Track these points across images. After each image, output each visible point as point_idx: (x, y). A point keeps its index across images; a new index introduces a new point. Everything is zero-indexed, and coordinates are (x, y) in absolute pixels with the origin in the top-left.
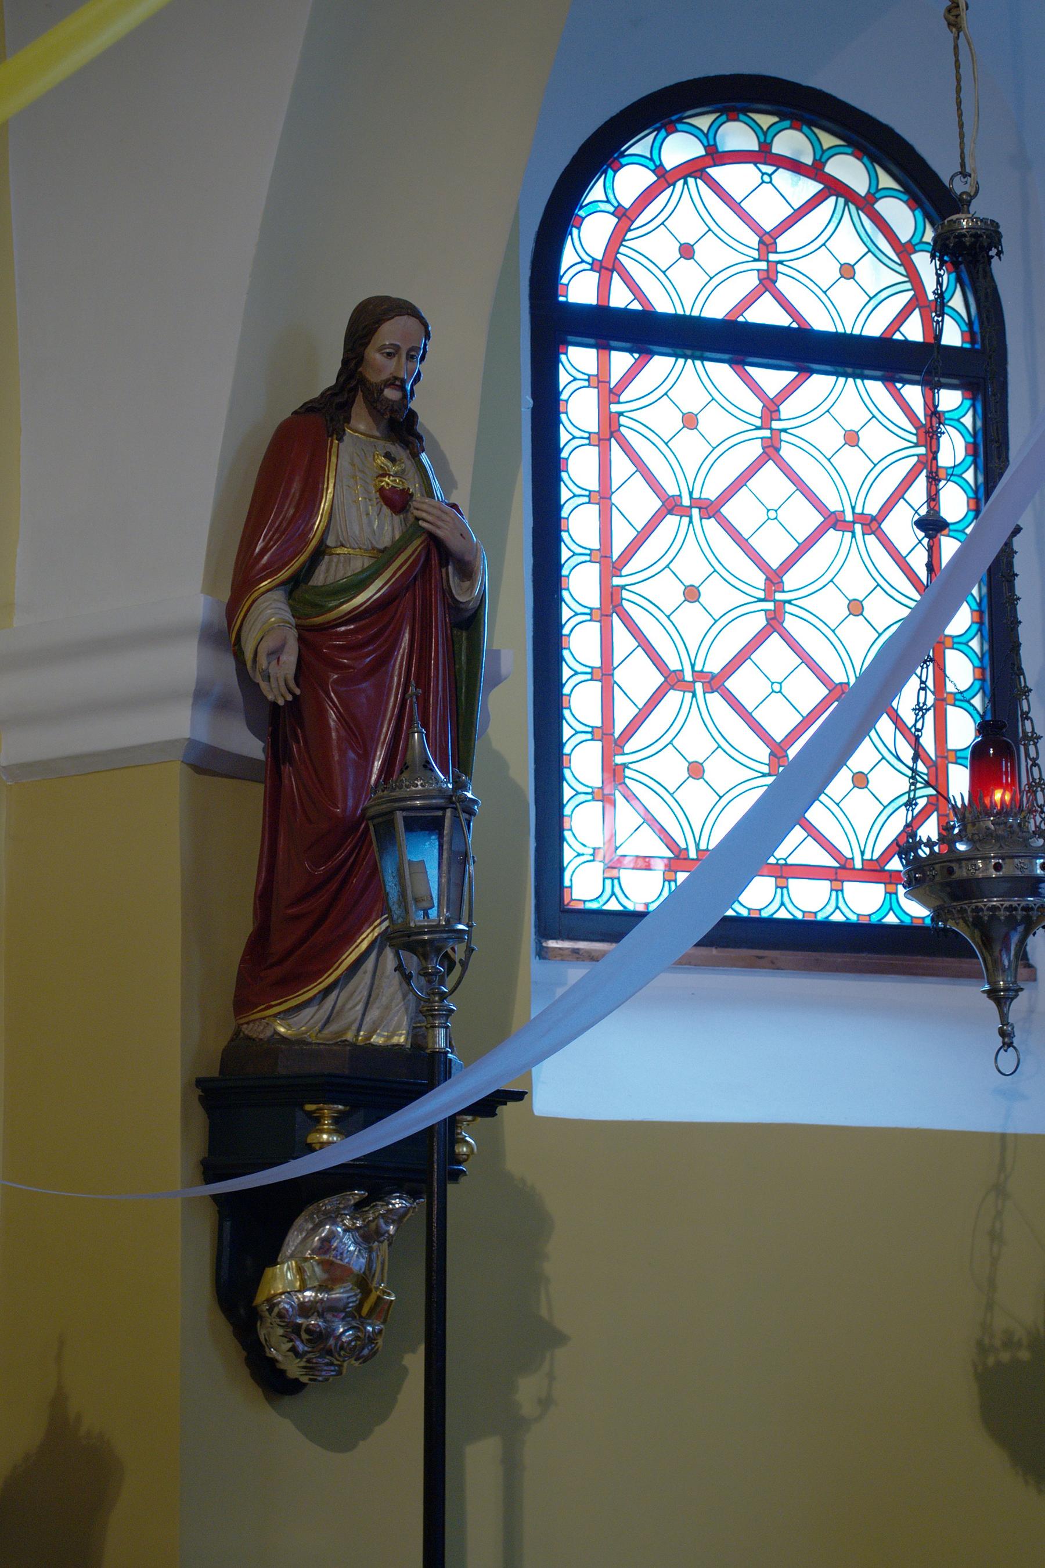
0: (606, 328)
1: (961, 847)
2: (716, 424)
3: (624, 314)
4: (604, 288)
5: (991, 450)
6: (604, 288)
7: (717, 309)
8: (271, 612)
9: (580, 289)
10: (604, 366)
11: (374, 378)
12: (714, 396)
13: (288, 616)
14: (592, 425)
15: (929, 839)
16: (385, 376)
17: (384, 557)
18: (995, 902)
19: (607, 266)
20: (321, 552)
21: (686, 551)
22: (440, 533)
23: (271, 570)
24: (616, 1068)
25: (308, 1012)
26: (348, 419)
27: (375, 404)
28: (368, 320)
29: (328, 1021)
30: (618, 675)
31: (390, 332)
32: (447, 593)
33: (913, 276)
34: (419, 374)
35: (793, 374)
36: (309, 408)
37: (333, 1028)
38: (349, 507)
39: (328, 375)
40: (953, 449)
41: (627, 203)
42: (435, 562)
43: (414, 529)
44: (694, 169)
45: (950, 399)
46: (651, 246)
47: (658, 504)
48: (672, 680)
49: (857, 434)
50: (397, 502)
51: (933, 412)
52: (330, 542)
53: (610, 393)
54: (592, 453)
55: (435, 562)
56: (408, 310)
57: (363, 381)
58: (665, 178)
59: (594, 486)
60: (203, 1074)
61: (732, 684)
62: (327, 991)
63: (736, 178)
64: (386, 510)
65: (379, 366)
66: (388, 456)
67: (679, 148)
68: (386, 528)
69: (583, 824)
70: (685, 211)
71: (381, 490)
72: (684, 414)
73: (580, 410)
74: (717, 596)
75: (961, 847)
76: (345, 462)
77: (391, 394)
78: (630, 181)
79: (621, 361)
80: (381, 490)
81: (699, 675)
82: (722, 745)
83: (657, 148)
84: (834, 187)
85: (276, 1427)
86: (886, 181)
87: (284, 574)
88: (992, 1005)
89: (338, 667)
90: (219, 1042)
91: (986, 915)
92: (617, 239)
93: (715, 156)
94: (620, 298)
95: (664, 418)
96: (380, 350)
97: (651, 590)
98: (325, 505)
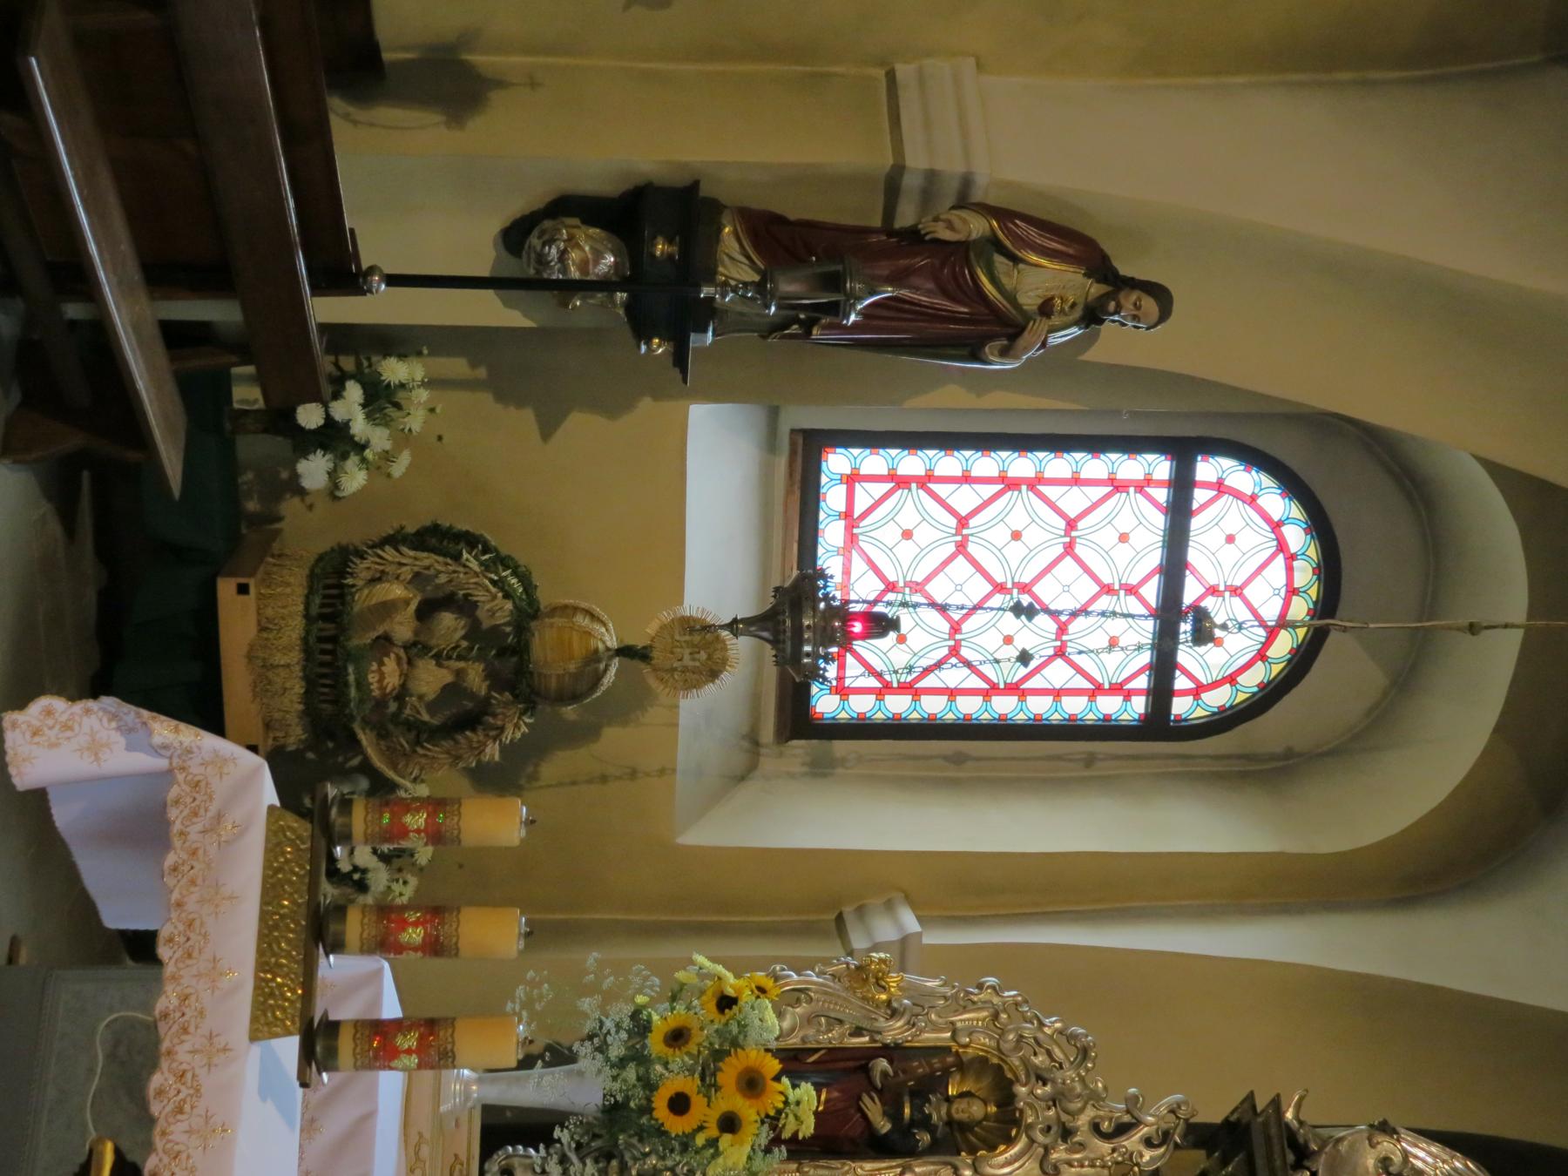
0: (1182, 485)
1: (822, 605)
2: (1123, 553)
3: (1188, 498)
4: (1206, 485)
5: (1106, 731)
6: (1206, 485)
7: (1193, 556)
8: (977, 226)
9: (1207, 469)
10: (1160, 484)
11: (1122, 296)
12: (1138, 556)
13: (974, 236)
14: (1120, 476)
15: (845, 626)
16: (1123, 301)
17: (1011, 298)
18: (788, 623)
19: (1220, 487)
20: (1015, 260)
21: (1044, 535)
22: (1026, 334)
23: (1003, 227)
24: (717, 452)
25: (736, 246)
26: (1098, 281)
27: (1103, 299)
28: (1160, 294)
29: (732, 258)
30: (966, 487)
31: (1150, 305)
32: (991, 337)
33: (1216, 684)
34: (1124, 325)
35: (1154, 605)
36: (1105, 259)
37: (726, 259)
38: (1041, 278)
39: (1125, 270)
40: (1109, 706)
41: (1259, 501)
42: (1010, 331)
43: (1027, 317)
44: (1282, 546)
45: (1139, 705)
46: (1231, 514)
47: (1072, 515)
48: (963, 522)
49: (1117, 650)
50: (1046, 309)
51: (1128, 695)
52: (1021, 266)
53: (1142, 486)
54: (1103, 474)
55: (1010, 331)
56: (1165, 314)
57: (1118, 289)
58: (1276, 526)
59: (1083, 476)
60: (702, 185)
61: (961, 558)
62: (748, 257)
63: (1276, 573)
64: (1040, 301)
65: (1129, 299)
66: (1073, 305)
67: (1296, 537)
68: (1029, 300)
69: (874, 462)
70: (1257, 540)
71: (1052, 298)
72: (1128, 535)
73: (1131, 467)
74: (1015, 551)
75: (822, 605)
76: (1070, 276)
77: (1112, 306)
78: (1252, 680)
79: (1162, 495)
80: (1052, 298)
81: (966, 538)
82: (923, 551)
83: (1295, 521)
84: (1272, 634)
85: (495, 224)
86: (1276, 669)
87: (1000, 234)
88: (728, 620)
89: (943, 266)
90: (724, 197)
91: (781, 618)
92: (1237, 495)
93: (1291, 558)
94: (1200, 496)
95: (1125, 522)
96: (1139, 299)
97: (1019, 509)
98: (1043, 261)
